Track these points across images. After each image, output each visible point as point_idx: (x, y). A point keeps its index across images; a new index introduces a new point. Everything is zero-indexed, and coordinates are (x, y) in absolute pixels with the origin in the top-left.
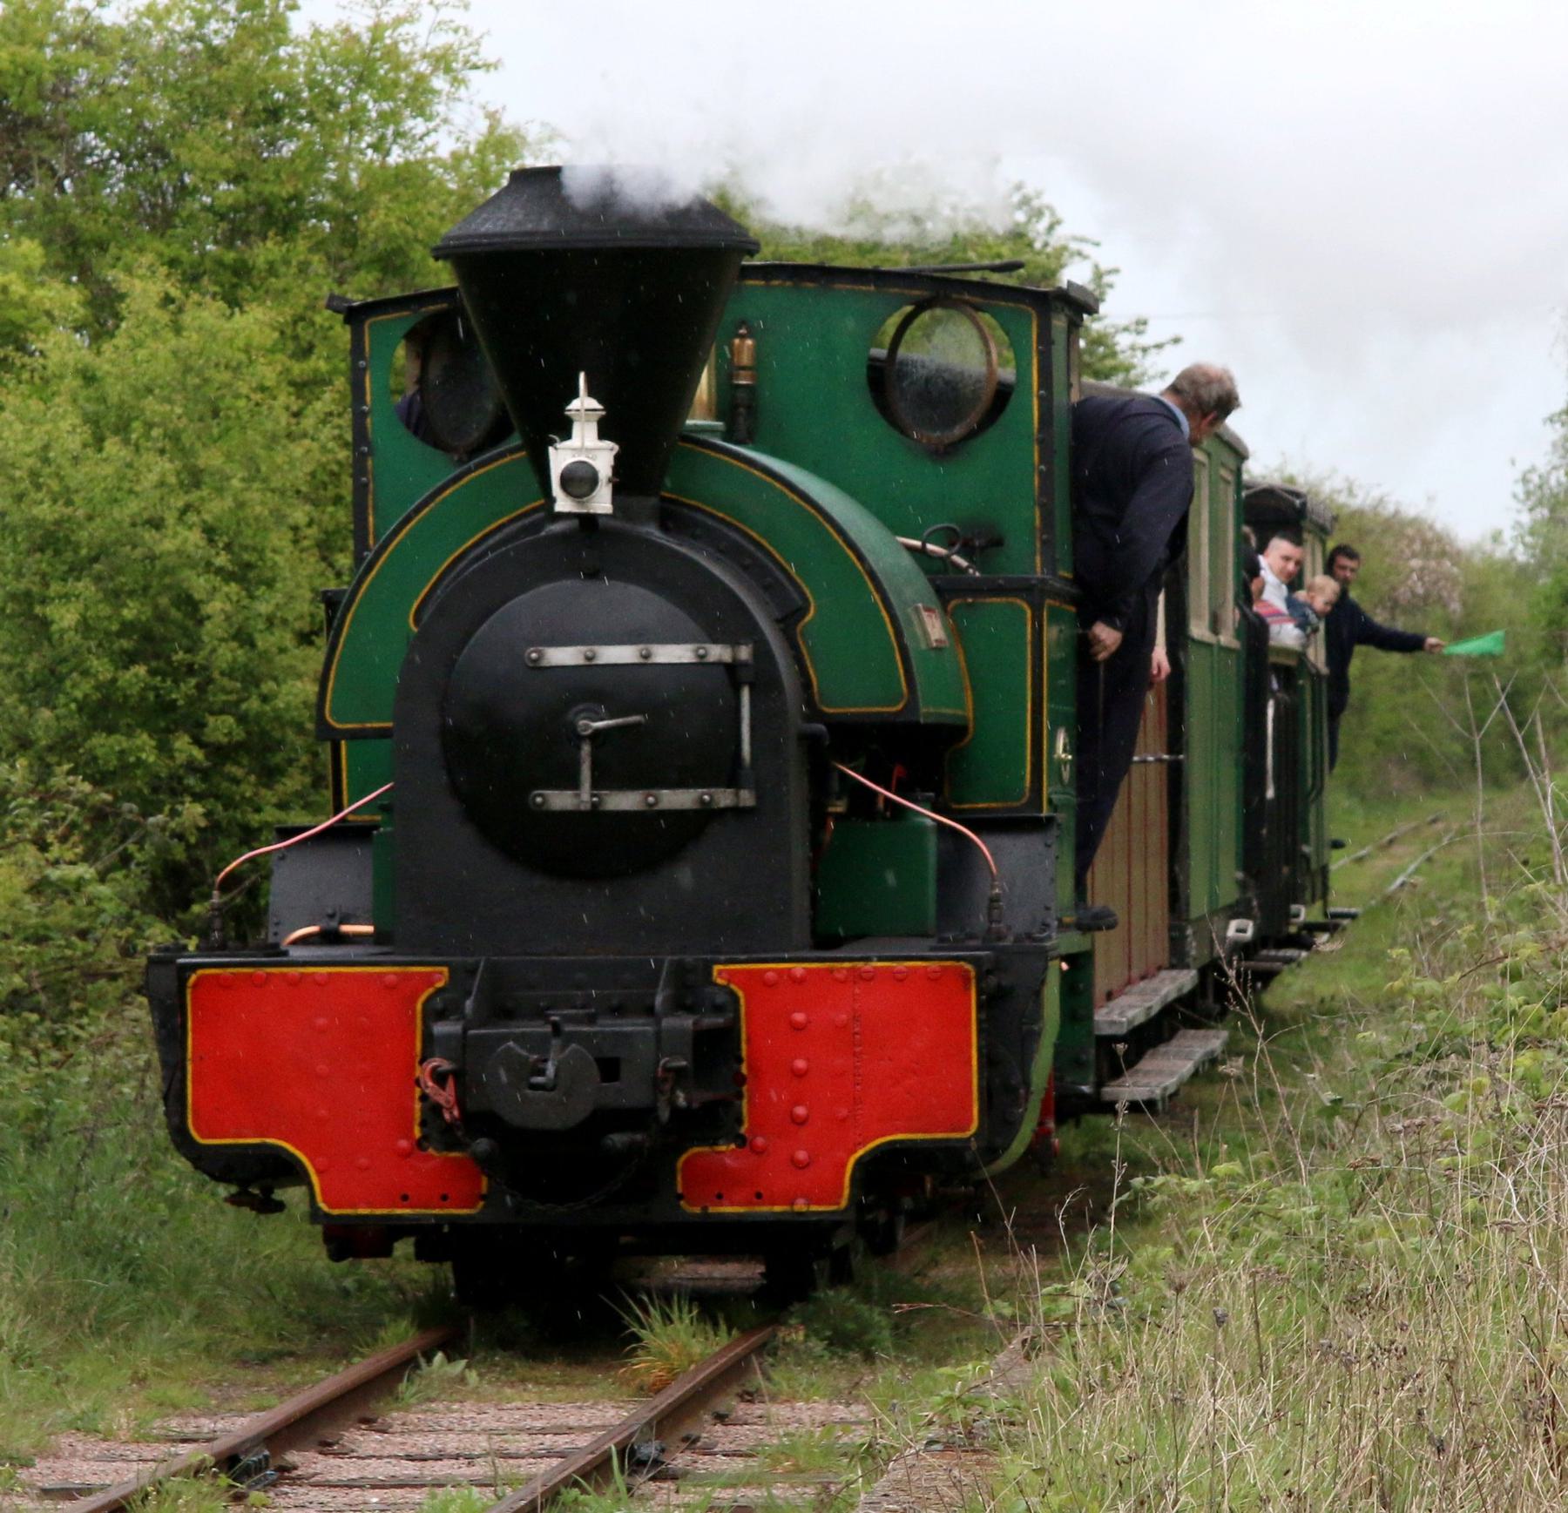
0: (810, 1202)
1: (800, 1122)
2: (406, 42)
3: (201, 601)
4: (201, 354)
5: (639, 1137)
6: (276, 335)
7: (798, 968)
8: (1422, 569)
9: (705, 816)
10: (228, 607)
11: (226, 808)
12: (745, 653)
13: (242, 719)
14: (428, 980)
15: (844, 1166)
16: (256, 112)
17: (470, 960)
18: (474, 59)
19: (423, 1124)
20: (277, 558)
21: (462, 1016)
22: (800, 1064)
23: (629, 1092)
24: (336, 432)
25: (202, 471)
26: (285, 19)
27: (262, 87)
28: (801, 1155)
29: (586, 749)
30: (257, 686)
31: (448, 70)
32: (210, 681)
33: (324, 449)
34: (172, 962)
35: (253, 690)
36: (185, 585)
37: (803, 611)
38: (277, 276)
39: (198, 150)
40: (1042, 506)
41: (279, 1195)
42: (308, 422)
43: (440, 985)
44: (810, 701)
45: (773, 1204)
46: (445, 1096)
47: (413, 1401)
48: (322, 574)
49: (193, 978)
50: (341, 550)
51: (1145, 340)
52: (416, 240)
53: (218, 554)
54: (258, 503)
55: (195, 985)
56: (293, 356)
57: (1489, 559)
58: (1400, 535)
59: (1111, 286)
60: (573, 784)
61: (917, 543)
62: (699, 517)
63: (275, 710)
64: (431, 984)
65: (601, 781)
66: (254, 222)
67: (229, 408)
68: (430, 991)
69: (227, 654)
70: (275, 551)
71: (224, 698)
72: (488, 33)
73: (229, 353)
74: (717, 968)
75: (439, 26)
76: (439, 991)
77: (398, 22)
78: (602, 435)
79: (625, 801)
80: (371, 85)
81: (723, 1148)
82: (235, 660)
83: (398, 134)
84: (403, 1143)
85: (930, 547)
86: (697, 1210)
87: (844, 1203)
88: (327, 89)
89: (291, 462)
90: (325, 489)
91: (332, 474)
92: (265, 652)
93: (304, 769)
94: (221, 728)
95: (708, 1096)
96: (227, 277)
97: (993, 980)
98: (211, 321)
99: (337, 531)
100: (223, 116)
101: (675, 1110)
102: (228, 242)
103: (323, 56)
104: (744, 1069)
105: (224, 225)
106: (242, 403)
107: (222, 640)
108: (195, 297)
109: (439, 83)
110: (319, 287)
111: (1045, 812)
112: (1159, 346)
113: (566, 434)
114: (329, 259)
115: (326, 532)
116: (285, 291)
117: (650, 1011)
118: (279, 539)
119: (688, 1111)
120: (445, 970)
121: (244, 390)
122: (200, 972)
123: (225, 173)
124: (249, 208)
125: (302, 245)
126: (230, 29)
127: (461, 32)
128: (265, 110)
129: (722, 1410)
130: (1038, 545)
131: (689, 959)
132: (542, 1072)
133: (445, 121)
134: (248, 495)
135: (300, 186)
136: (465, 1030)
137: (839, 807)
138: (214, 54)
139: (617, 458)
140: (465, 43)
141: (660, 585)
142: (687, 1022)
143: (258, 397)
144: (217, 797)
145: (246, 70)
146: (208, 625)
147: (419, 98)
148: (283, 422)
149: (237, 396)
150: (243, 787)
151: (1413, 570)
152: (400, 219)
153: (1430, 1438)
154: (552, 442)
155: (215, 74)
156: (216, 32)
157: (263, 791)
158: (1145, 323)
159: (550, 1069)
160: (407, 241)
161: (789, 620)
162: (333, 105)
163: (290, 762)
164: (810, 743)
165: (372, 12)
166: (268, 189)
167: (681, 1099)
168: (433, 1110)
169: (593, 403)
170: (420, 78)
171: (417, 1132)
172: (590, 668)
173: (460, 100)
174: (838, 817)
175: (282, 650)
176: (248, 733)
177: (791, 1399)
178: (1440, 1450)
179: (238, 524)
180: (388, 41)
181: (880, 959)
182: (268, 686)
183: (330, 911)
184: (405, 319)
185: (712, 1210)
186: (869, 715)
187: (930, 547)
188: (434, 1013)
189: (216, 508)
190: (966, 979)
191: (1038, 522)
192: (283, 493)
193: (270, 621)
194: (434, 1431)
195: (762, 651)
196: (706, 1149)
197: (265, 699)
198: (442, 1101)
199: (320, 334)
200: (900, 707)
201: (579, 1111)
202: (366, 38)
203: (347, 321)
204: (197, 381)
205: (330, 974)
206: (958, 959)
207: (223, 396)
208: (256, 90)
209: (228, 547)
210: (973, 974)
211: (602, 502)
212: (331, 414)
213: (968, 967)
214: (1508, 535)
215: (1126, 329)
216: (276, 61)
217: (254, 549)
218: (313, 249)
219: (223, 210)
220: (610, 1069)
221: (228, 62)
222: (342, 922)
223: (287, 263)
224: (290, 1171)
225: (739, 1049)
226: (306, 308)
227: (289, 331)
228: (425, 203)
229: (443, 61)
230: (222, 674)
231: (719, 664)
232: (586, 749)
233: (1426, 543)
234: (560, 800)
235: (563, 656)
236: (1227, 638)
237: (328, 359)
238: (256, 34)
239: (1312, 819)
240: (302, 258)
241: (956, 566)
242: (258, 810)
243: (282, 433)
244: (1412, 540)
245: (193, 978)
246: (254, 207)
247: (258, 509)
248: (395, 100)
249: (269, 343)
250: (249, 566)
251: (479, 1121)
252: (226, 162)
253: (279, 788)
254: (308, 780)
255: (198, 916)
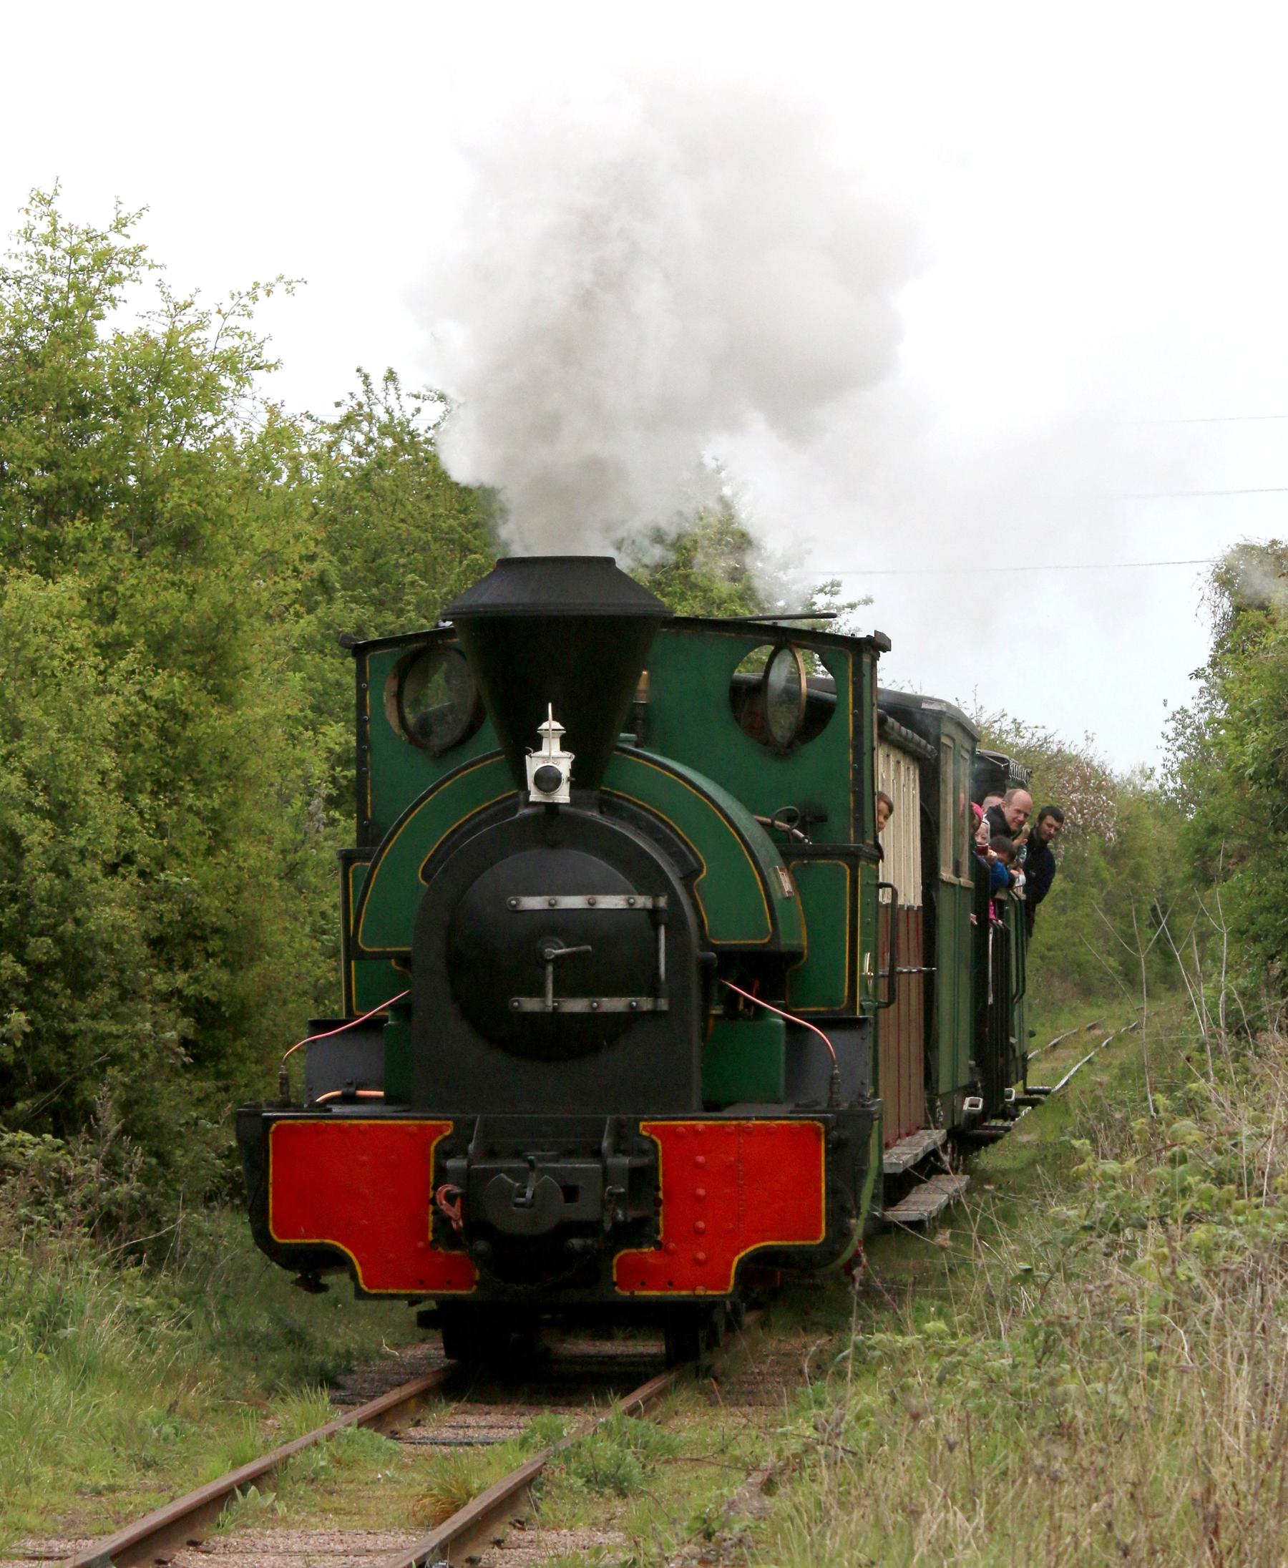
0: (707, 1289)
1: (699, 1233)
2: (197, 346)
3: (23, 837)
4: (20, 621)
5: (589, 1242)
6: (84, 603)
7: (700, 1124)
8: (1081, 802)
9: (632, 1016)
10: (45, 841)
11: (45, 1018)
12: (662, 902)
13: (59, 941)
14: (439, 1130)
15: (729, 1264)
16: (68, 408)
17: (470, 1116)
18: (257, 360)
19: (434, 1231)
20: (88, 799)
21: (466, 1154)
22: (701, 1192)
23: (585, 1210)
24: (138, 687)
25: (23, 723)
26: (93, 328)
27: (72, 386)
28: (701, 1256)
29: (550, 968)
30: (72, 911)
31: (234, 370)
32: (32, 906)
33: (128, 702)
34: (258, 1115)
35: (68, 914)
36: (9, 822)
37: (699, 871)
38: (84, 552)
39: (16, 442)
40: (855, 793)
41: (326, 1280)
42: (112, 680)
43: (447, 1133)
44: (703, 936)
45: (681, 1289)
46: (454, 1212)
47: (232, 1527)
48: (127, 813)
49: (274, 1126)
50: (140, 792)
51: (839, 600)
52: (207, 519)
53: (37, 795)
54: (71, 750)
55: (274, 1132)
56: (99, 622)
57: (1138, 792)
58: (1061, 770)
59: (810, 552)
60: (541, 993)
61: (769, 820)
62: (625, 804)
63: (89, 932)
64: (441, 1133)
65: (562, 990)
66: (64, 503)
67: (45, 668)
68: (440, 1138)
69: (44, 882)
70: (86, 793)
71: (43, 922)
72: (270, 338)
73: (45, 619)
74: (642, 1124)
75: (226, 332)
76: (447, 1138)
77: (191, 328)
78: (563, 748)
79: (577, 1005)
80: (166, 384)
81: (646, 1250)
82: (52, 887)
83: (189, 426)
84: (421, 1244)
85: (777, 823)
86: (628, 1294)
87: (730, 1289)
88: (129, 387)
89: (99, 713)
90: (127, 737)
91: (132, 724)
92: (79, 881)
93: (113, 984)
94: (41, 948)
95: (633, 1214)
96: (42, 552)
97: (835, 1134)
98: (30, 592)
99: (136, 774)
100: (37, 410)
101: (616, 1224)
102: (42, 521)
103: (126, 359)
104: (661, 1195)
105: (39, 507)
106: (56, 663)
107: (44, 871)
108: (15, 571)
109: (226, 381)
110: (122, 561)
111: (859, 1015)
112: (852, 606)
113: (538, 747)
114: (130, 536)
115: (127, 775)
116: (91, 564)
117: (597, 1154)
118: (89, 782)
119: (625, 1224)
120: (451, 1123)
121: (59, 652)
122: (279, 1122)
123: (40, 461)
124: (60, 491)
125: (106, 524)
126: (44, 336)
127: (246, 337)
128: (74, 406)
129: (499, 1536)
130: (852, 820)
131: (623, 1117)
132: (523, 1195)
133: (231, 414)
134: (62, 744)
135: (105, 473)
136: (469, 1166)
137: (717, 1010)
138: (32, 360)
139: (573, 763)
140: (250, 347)
141: (607, 855)
142: (625, 1161)
143: (68, 657)
144: (37, 1009)
145: (58, 371)
146: (29, 856)
147: (209, 395)
148: (92, 681)
149: (52, 657)
150: (60, 998)
151: (1073, 803)
152: (191, 501)
153: (1118, 1544)
154: (528, 752)
155: (31, 376)
156: (32, 339)
157: (78, 1004)
158: (839, 585)
159: (529, 1193)
160: (198, 518)
161: (690, 876)
162: (134, 401)
163: (101, 978)
164: (705, 966)
165: (168, 321)
166: (76, 475)
167: (620, 1216)
168: (443, 1221)
169: (557, 725)
170: (210, 377)
171: (430, 1237)
172: (552, 912)
173: (244, 396)
174: (716, 1016)
175: (94, 880)
176: (64, 952)
177: (557, 1527)
178: (1126, 1554)
179: (55, 770)
180: (182, 345)
181: (757, 1119)
182: (80, 912)
183: (348, 1080)
184: (396, 653)
185: (637, 1293)
186: (741, 946)
187: (777, 823)
188: (444, 1153)
189: (33, 755)
190: (817, 1132)
191: (852, 805)
192: (92, 742)
193: (82, 853)
194: (251, 1552)
195: (674, 900)
196: (634, 1251)
197: (78, 922)
198: (451, 1214)
199: (122, 603)
200: (766, 940)
201: (547, 1223)
202: (162, 343)
203: (354, 655)
204: (17, 644)
205: (370, 1125)
206: (813, 1119)
207: (41, 657)
208: (67, 389)
209: (46, 789)
210: (823, 1130)
211: (563, 795)
212: (133, 672)
213: (819, 1124)
214: (1159, 772)
215: (821, 591)
216: (84, 364)
217: (69, 791)
218: (116, 528)
219: (38, 494)
220: (571, 1193)
221: (42, 365)
222: (358, 1089)
223: (94, 540)
224: (337, 1261)
225: (657, 1180)
226: (110, 579)
227: (95, 599)
228: (215, 486)
229: (229, 362)
230: (42, 900)
231: (644, 909)
232: (550, 968)
233: (1085, 780)
234: (530, 1004)
235: (534, 903)
236: (965, 881)
237: (129, 623)
238: (67, 340)
239: (1016, 1014)
240: (106, 534)
241: (796, 837)
242: (73, 1020)
243: (91, 689)
244: (1073, 776)
245: (274, 1126)
246: (64, 490)
247: (72, 756)
248: (187, 397)
249: (79, 609)
250: (63, 806)
251: (478, 1227)
252: (40, 452)
253: (91, 1000)
254: (116, 993)
255: (22, 1112)
